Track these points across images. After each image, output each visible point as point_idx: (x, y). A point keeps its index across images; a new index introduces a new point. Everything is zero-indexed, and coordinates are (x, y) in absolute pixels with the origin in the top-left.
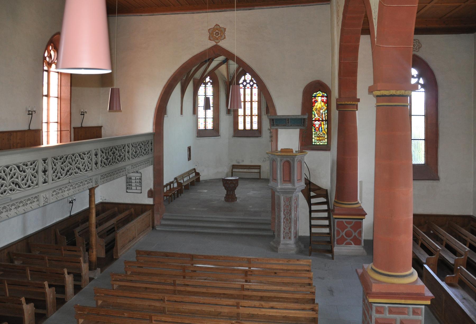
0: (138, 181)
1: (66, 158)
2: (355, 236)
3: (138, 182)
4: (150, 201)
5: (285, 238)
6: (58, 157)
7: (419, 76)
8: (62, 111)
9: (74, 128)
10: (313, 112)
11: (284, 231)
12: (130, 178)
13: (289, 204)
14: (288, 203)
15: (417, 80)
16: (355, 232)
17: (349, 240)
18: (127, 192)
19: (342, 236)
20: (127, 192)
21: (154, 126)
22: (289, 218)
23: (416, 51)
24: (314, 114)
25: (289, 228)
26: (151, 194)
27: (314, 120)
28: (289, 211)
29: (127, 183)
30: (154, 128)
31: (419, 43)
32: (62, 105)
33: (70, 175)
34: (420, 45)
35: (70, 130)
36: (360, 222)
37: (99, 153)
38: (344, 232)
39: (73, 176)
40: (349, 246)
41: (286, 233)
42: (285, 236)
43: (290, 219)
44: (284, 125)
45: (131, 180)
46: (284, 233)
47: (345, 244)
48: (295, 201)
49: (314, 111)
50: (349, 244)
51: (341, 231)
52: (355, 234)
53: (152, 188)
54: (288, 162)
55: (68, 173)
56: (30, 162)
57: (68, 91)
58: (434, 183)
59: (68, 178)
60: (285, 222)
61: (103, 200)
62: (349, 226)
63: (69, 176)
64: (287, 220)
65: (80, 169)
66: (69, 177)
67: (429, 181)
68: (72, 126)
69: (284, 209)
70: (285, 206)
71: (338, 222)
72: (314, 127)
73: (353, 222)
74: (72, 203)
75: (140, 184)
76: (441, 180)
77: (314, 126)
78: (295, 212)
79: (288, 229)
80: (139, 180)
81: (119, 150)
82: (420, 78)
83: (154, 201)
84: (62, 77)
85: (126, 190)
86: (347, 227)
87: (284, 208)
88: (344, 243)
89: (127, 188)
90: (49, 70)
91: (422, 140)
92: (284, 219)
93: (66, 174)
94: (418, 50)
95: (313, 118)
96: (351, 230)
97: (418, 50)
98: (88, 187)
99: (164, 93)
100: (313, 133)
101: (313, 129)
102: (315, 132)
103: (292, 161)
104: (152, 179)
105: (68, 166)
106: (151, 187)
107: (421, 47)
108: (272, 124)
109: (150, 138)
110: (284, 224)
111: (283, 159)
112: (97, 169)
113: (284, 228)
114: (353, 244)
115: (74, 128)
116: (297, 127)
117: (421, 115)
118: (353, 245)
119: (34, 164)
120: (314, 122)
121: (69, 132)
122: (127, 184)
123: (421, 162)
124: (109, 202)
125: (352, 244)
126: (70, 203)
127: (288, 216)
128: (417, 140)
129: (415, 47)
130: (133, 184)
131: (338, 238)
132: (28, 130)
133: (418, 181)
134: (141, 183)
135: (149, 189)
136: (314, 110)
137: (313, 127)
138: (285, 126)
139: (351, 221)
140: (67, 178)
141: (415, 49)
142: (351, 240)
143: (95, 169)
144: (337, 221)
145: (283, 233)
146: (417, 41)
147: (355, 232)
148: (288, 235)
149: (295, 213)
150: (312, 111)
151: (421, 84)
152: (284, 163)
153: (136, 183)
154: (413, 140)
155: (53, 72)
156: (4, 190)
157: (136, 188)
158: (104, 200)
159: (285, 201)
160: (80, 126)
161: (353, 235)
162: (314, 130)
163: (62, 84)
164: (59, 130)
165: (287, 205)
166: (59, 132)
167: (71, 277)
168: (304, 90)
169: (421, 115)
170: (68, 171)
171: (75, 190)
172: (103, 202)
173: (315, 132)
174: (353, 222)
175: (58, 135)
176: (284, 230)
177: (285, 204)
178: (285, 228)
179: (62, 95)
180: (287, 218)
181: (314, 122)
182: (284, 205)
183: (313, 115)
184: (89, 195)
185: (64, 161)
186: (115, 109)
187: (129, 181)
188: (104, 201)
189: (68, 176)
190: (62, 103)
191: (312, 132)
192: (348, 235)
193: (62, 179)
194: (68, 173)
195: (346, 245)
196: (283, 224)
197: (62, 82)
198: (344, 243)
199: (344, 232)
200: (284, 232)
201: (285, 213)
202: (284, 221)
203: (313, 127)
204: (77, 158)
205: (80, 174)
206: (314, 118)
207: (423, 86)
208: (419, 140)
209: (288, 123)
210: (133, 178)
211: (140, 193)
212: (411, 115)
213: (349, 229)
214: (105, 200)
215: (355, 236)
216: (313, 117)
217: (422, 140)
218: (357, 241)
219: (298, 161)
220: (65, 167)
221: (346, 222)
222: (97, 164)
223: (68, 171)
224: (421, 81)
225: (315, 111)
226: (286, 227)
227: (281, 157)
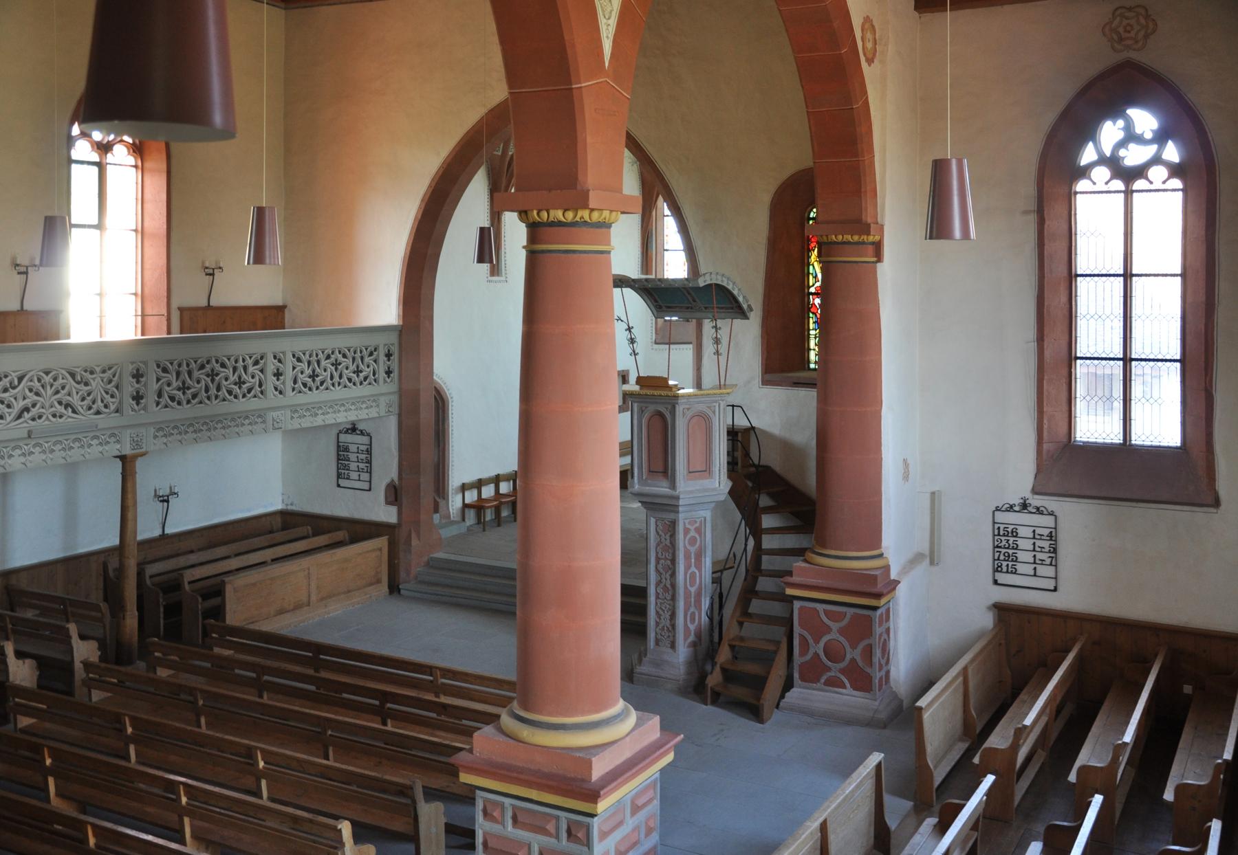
0: (363, 456)
1: (20, 379)
2: (853, 660)
3: (362, 460)
4: (388, 515)
5: (660, 643)
6: (96, 368)
7: (1161, 137)
8: (147, 266)
9: (181, 310)
10: (811, 267)
11: (657, 622)
12: (347, 449)
13: (671, 543)
14: (668, 541)
15: (1151, 150)
16: (854, 647)
17: (835, 670)
18: (339, 486)
19: (816, 654)
20: (339, 486)
21: (401, 307)
22: (669, 583)
23: (1134, 50)
24: (812, 274)
25: (670, 613)
26: (394, 495)
27: (812, 294)
28: (669, 562)
29: (340, 462)
30: (401, 314)
31: (1147, 17)
32: (146, 249)
33: (33, 419)
34: (1151, 26)
35: (166, 314)
36: (869, 616)
37: (152, 373)
38: (822, 644)
39: (47, 422)
40: (836, 689)
41: (663, 629)
42: (659, 637)
43: (674, 586)
44: (688, 308)
45: (348, 453)
46: (657, 630)
47: (826, 684)
48: (692, 533)
49: (813, 265)
50: (834, 683)
51: (811, 641)
52: (853, 654)
53: (396, 479)
54: (661, 415)
55: (26, 413)
56: (100, 368)
57: (160, 213)
58: (1199, 516)
59: (25, 425)
60: (659, 594)
61: (287, 505)
62: (835, 626)
63: (30, 422)
64: (665, 589)
65: (72, 407)
66: (27, 423)
67: (1186, 508)
68: (175, 304)
69: (657, 555)
70: (661, 546)
71: (801, 609)
72: (813, 313)
73: (848, 616)
74: (167, 501)
75: (367, 465)
76: (1223, 507)
77: (812, 310)
78: (693, 569)
79: (668, 616)
80: (367, 456)
81: (341, 377)
82: (1168, 141)
83: (400, 513)
84: (145, 179)
85: (335, 479)
86: (829, 630)
87: (657, 553)
88: (822, 681)
89: (339, 476)
90: (104, 161)
91: (1170, 361)
92: (657, 584)
93: (19, 416)
94: (1140, 43)
95: (809, 287)
96: (842, 639)
97: (1140, 43)
98: (101, 453)
99: (422, 215)
100: (809, 334)
101: (811, 319)
102: (816, 330)
103: (670, 413)
104: (395, 452)
105: (24, 399)
106: (393, 474)
107: (1154, 31)
108: (37, 268)
109: (381, 341)
110: (659, 601)
111: (646, 407)
112: (142, 412)
113: (657, 612)
114: (848, 685)
115: (181, 310)
116: (723, 314)
117: (1166, 275)
118: (849, 690)
119: (89, 398)
120: (814, 300)
121: (164, 319)
122: (340, 465)
123: (1112, 436)
124: (300, 510)
125: (844, 687)
126: (163, 501)
127: (668, 577)
128: (1150, 360)
129: (1132, 34)
130: (353, 466)
131: (803, 660)
132: (18, 311)
133: (1134, 504)
134: (369, 462)
135: (388, 480)
136: (813, 260)
137: (811, 315)
138: (690, 310)
139: (842, 613)
140: (21, 426)
141: (1129, 42)
142: (842, 671)
143: (133, 410)
144: (798, 606)
145: (656, 628)
146: (1143, 11)
147: (854, 647)
148: (667, 634)
149: (693, 573)
150: (809, 265)
151: (1168, 165)
152: (649, 420)
153: (358, 464)
154: (1082, 361)
155: (85, 166)
156: (40, 412)
157: (359, 475)
158: (289, 503)
159: (660, 532)
160: (204, 303)
161: (848, 657)
162: (814, 322)
163: (148, 196)
164: (140, 313)
165: (666, 545)
166: (139, 319)
167: (26, 665)
168: (772, 201)
169: (1166, 275)
170: (27, 409)
171: (51, 456)
172: (287, 510)
173: (816, 330)
174: (846, 613)
175: (136, 327)
176: (658, 621)
177: (661, 542)
178: (661, 612)
179: (146, 224)
180: (665, 585)
181: (814, 300)
182: (658, 545)
183: (811, 277)
184: (121, 476)
185: (11, 384)
186: (267, 261)
187: (344, 455)
188: (290, 508)
189: (26, 422)
190: (146, 244)
191: (809, 330)
192: (833, 654)
193: (5, 428)
194: (26, 413)
195: (827, 688)
196: (656, 603)
197: (146, 191)
198: (822, 681)
199: (822, 644)
200: (657, 624)
201: (660, 567)
202: (658, 591)
203: (811, 315)
204: (60, 381)
205: (70, 420)
206: (813, 285)
207: (1176, 171)
208: (1158, 360)
209: (694, 301)
210: (353, 448)
211: (367, 490)
212: (1183, 275)
213: (834, 635)
214: (292, 504)
215: (853, 660)
216: (811, 284)
217: (1170, 361)
218: (862, 680)
219: (690, 414)
220: (15, 399)
221: (826, 612)
222: (142, 399)
223: (27, 409)
224: (1172, 153)
225: (816, 264)
226: (663, 611)
227: (642, 402)
